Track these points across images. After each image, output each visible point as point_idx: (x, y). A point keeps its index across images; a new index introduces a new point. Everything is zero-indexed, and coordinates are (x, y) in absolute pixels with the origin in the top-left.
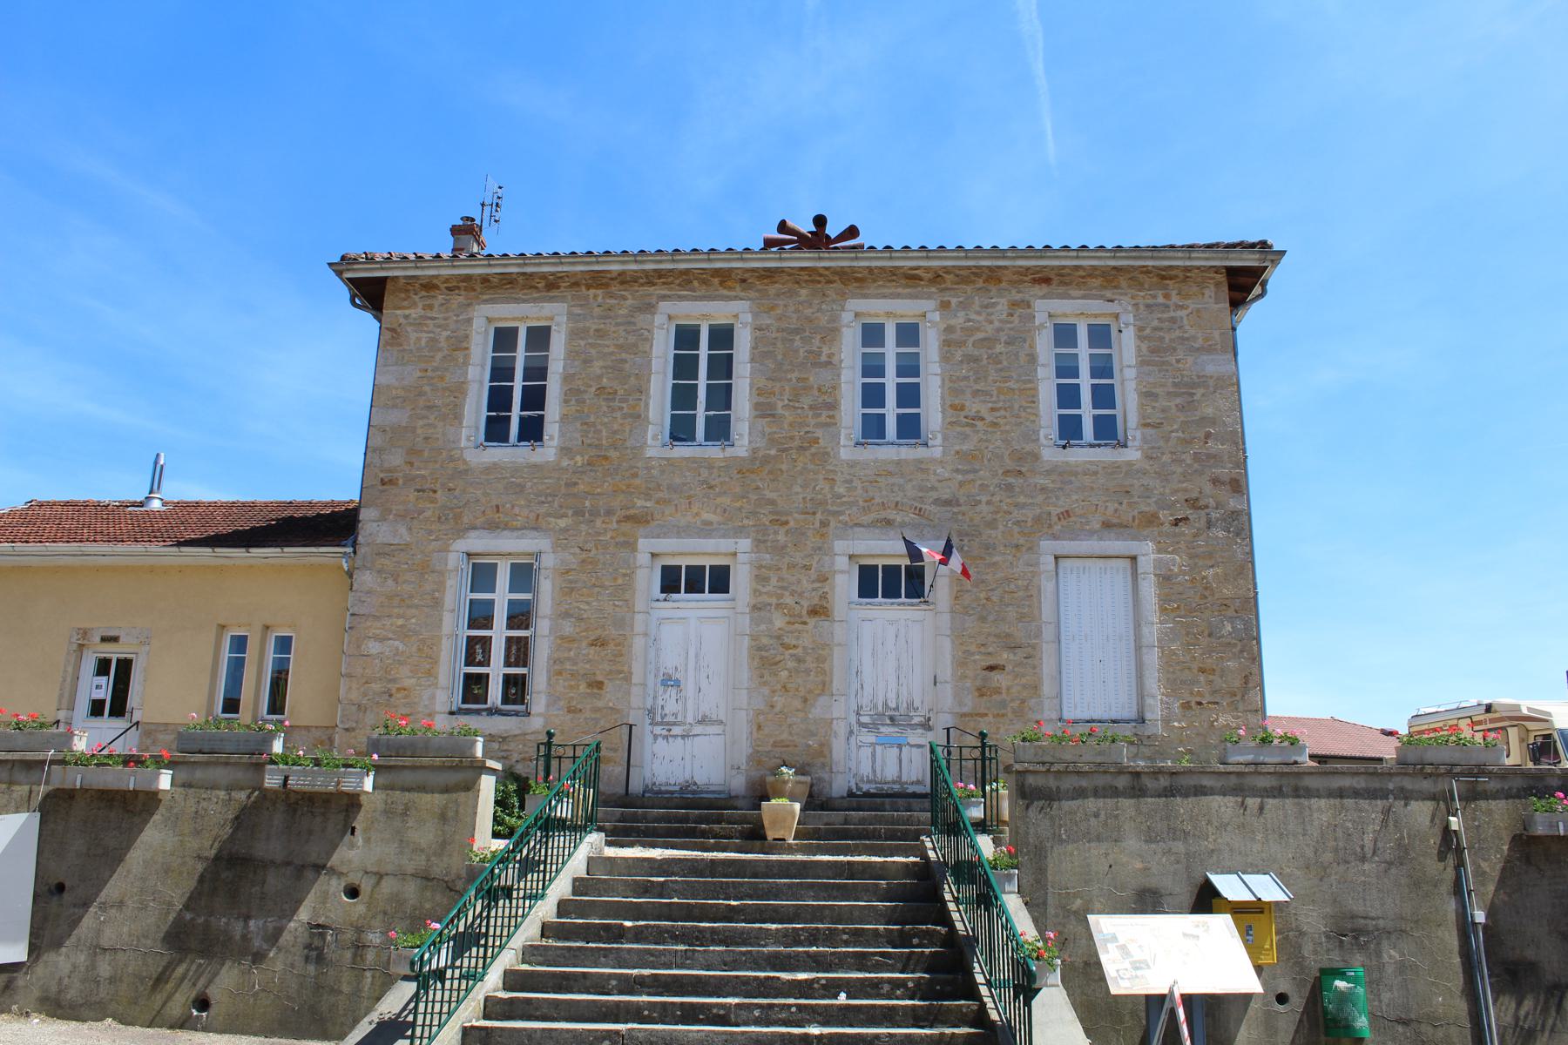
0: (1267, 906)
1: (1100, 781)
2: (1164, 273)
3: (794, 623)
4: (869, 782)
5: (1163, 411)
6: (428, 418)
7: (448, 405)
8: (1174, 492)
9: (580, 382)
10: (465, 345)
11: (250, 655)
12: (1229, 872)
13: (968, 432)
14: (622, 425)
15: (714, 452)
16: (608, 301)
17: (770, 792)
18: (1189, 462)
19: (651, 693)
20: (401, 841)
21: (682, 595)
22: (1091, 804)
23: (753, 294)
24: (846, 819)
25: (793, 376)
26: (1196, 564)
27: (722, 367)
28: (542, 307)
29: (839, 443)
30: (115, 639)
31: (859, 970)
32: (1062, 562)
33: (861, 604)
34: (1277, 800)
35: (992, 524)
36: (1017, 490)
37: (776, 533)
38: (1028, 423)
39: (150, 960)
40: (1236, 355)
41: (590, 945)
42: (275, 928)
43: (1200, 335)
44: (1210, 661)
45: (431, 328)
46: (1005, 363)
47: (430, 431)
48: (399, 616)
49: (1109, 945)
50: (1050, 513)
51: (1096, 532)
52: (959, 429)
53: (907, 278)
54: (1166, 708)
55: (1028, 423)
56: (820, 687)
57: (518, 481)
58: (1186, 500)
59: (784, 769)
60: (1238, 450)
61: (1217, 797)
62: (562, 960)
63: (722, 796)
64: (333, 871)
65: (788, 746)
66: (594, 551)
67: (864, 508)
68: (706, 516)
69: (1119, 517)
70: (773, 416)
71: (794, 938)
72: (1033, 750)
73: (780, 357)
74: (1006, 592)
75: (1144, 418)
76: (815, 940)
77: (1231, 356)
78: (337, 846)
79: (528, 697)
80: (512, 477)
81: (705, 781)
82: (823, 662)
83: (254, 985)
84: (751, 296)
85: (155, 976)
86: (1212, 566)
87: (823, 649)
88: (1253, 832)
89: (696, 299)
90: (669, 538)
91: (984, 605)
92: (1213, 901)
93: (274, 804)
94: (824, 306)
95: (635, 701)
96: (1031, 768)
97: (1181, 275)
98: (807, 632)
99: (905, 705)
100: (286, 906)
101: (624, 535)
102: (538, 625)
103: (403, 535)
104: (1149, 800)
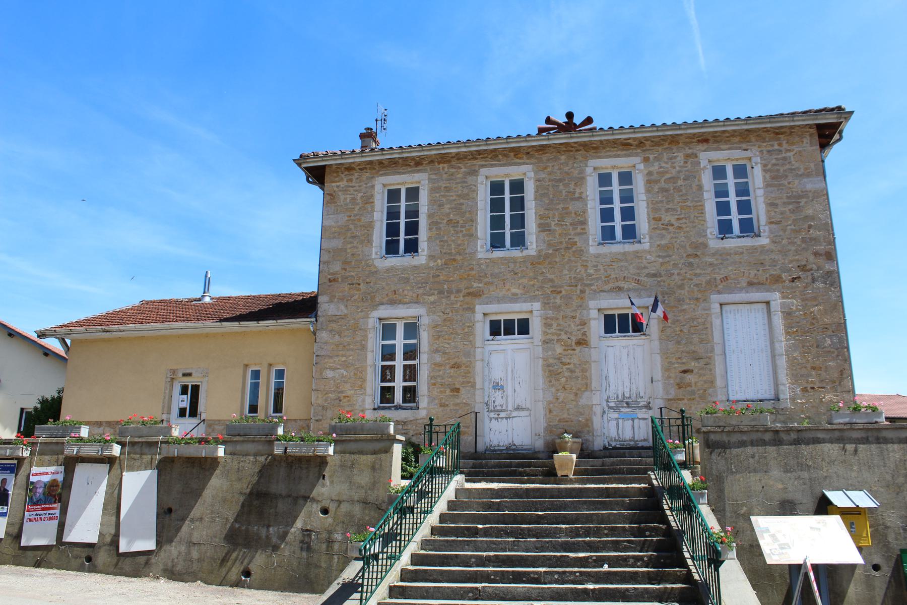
0: (862, 511)
1: (755, 436)
2: (777, 131)
3: (568, 350)
4: (616, 441)
7: (364, 235)
8: (791, 262)
9: (437, 218)
10: (371, 200)
11: (262, 381)
14: (463, 240)
16: (450, 170)
17: (558, 448)
18: (799, 243)
19: (487, 393)
22: (750, 450)
23: (533, 161)
26: (806, 304)
27: (518, 204)
28: (414, 176)
29: (588, 244)
30: (190, 375)
31: (615, 551)
32: (725, 307)
33: (606, 337)
36: (696, 266)
37: (555, 298)
38: (699, 226)
40: (825, 177)
41: (459, 539)
42: (283, 532)
44: (818, 362)
45: (351, 192)
46: (684, 191)
48: (343, 356)
49: (765, 535)
51: (744, 288)
52: (658, 232)
53: (623, 145)
54: (792, 392)
55: (699, 226)
56: (585, 386)
58: (799, 266)
59: (566, 435)
61: (827, 444)
63: (530, 452)
64: (314, 500)
66: (451, 314)
67: (605, 281)
68: (514, 290)
69: (758, 278)
70: (549, 230)
71: (576, 533)
72: (712, 419)
73: (551, 196)
75: (770, 219)
80: (402, 274)
81: (521, 443)
85: (221, 558)
86: (817, 305)
88: (851, 465)
90: (493, 304)
91: (679, 335)
94: (575, 165)
95: (478, 398)
96: (712, 430)
97: (788, 131)
98: (576, 355)
99: (635, 395)
100: (289, 520)
103: (342, 309)
104: (785, 447)
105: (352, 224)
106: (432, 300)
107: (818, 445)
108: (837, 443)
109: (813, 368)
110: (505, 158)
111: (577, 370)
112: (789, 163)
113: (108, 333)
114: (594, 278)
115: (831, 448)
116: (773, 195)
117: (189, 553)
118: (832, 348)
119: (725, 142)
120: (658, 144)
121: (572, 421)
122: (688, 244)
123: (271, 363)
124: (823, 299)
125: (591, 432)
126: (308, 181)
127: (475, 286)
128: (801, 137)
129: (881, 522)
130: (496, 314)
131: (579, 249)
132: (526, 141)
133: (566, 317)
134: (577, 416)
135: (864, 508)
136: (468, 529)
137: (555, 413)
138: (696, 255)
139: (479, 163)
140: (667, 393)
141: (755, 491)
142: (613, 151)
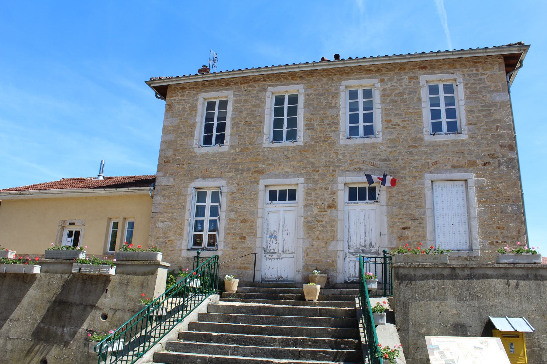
0: (520, 334)
1: (436, 271)
2: (475, 61)
3: (321, 212)
4: (353, 277)
5: (477, 118)
6: (182, 137)
7: (189, 132)
8: (483, 151)
9: (238, 120)
10: (195, 109)
11: (119, 229)
12: (502, 316)
13: (393, 131)
14: (254, 135)
15: (290, 144)
16: (249, 88)
17: (310, 280)
18: (489, 138)
19: (265, 241)
20: (125, 296)
21: (278, 202)
22: (431, 282)
23: (304, 82)
24: (341, 292)
25: (321, 112)
26: (494, 182)
27: (293, 111)
28: (224, 93)
29: (339, 138)
30: (74, 224)
31: (313, 359)
32: (435, 183)
33: (349, 203)
34: (526, 281)
35: (404, 168)
36: (414, 153)
37: (314, 175)
38: (418, 126)
39: (26, 343)
40: (509, 93)
41: (198, 343)
42: (74, 331)
43: (492, 85)
44: (502, 223)
45: (183, 104)
46: (408, 102)
47: (182, 142)
48: (170, 213)
49: (435, 352)
50: (429, 163)
51: (449, 170)
52: (389, 130)
53: (366, 71)
54: (482, 245)
55: (418, 126)
56: (332, 237)
57: (214, 159)
58: (489, 155)
59: (315, 271)
60: (512, 132)
61: (494, 279)
62: (182, 349)
63: (293, 283)
64: (98, 308)
65: (319, 262)
66: (243, 185)
67: (350, 164)
68: (287, 170)
69: (459, 163)
70: (313, 129)
71: (286, 343)
72: (403, 257)
73: (315, 105)
74: (410, 196)
75: (469, 121)
76: (296, 344)
77: (507, 93)
78: (100, 297)
79: (217, 243)
80: (212, 158)
81: (286, 277)
82: (334, 227)
83: (64, 355)
84: (303, 82)
85: (27, 350)
86: (501, 183)
87: (333, 222)
88: (514, 297)
89: (282, 85)
90: (272, 179)
91: (401, 202)
92: (493, 330)
93: (78, 280)
94: (333, 84)
95: (258, 244)
96: (401, 265)
97: (483, 61)
98: (327, 215)
99: (368, 245)
100: (79, 322)
101: (254, 178)
102: (221, 214)
103: (172, 181)
104: (460, 281)
105: (182, 124)
106: (231, 175)
107: (487, 280)
108: (503, 279)
109: (498, 228)
110: (286, 80)
111: (328, 226)
112: (483, 83)
113: (23, 196)
114: (343, 162)
115: (497, 283)
116: (471, 105)
117: (5, 345)
118: (512, 213)
119: (438, 68)
120: (391, 70)
121: (322, 262)
122: (410, 139)
123: (126, 217)
124: (506, 178)
125: (335, 270)
126: (157, 96)
127: (260, 166)
128: (493, 65)
129: (537, 345)
130: (274, 186)
131: (332, 141)
132: (299, 67)
133: (322, 188)
134: (326, 258)
135: (522, 333)
136: (205, 335)
137: (310, 256)
138: (415, 146)
139: (268, 83)
140: (391, 243)
141: (434, 315)
142: (359, 75)
